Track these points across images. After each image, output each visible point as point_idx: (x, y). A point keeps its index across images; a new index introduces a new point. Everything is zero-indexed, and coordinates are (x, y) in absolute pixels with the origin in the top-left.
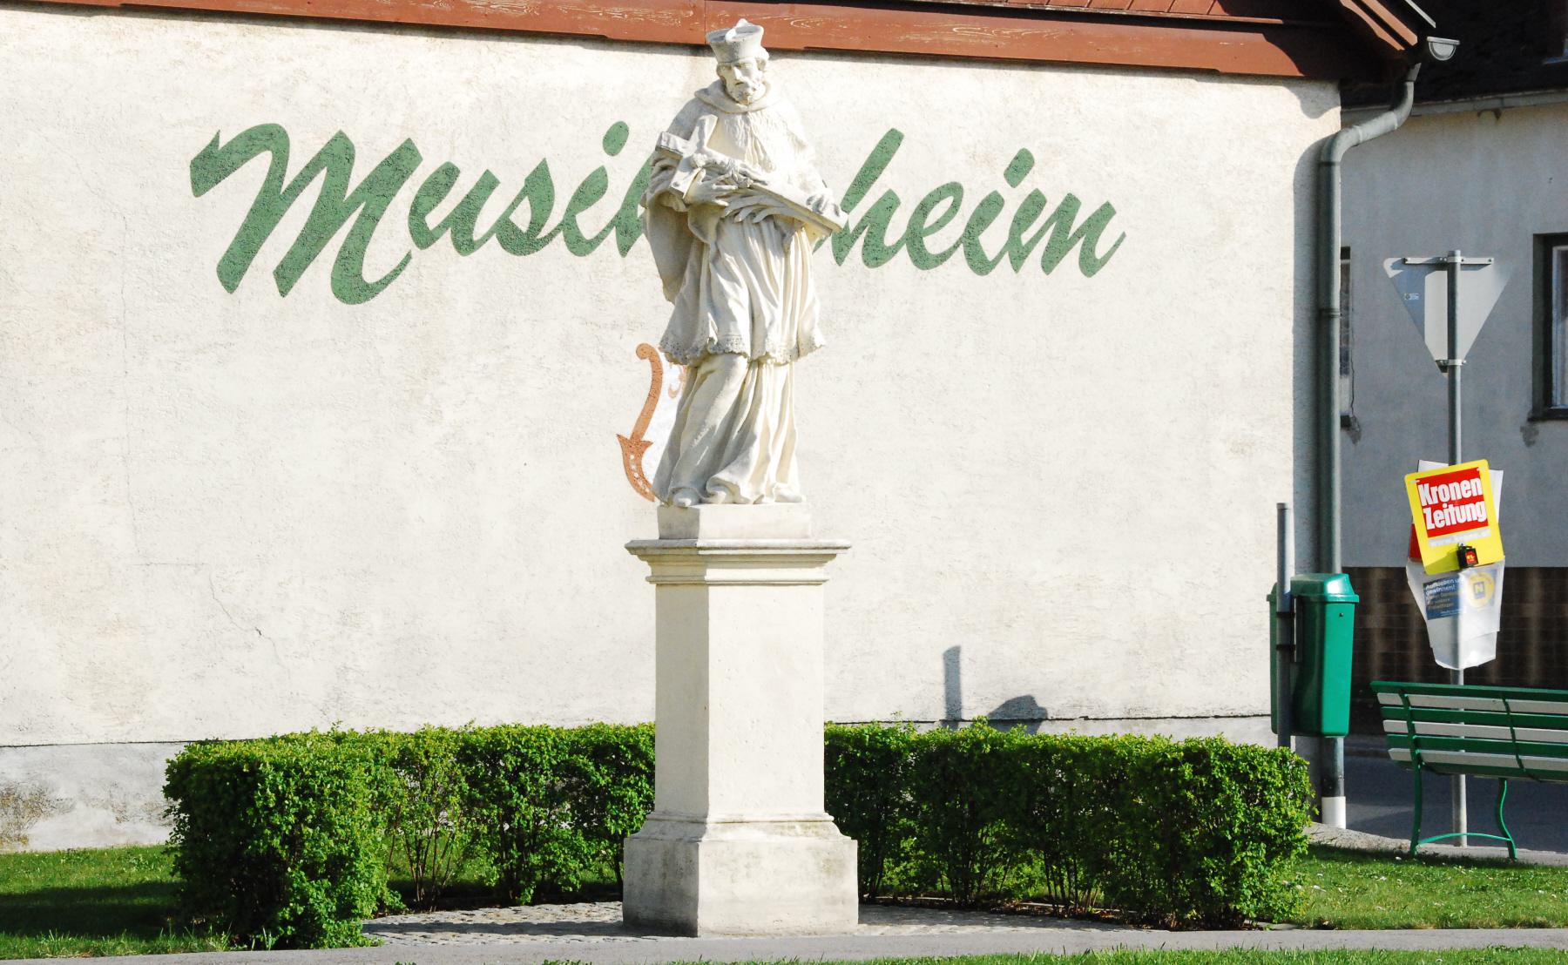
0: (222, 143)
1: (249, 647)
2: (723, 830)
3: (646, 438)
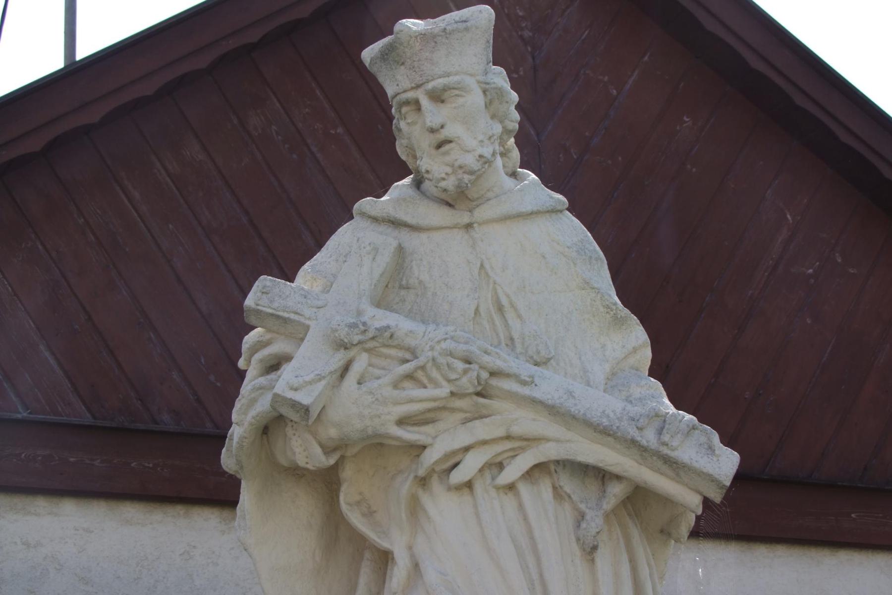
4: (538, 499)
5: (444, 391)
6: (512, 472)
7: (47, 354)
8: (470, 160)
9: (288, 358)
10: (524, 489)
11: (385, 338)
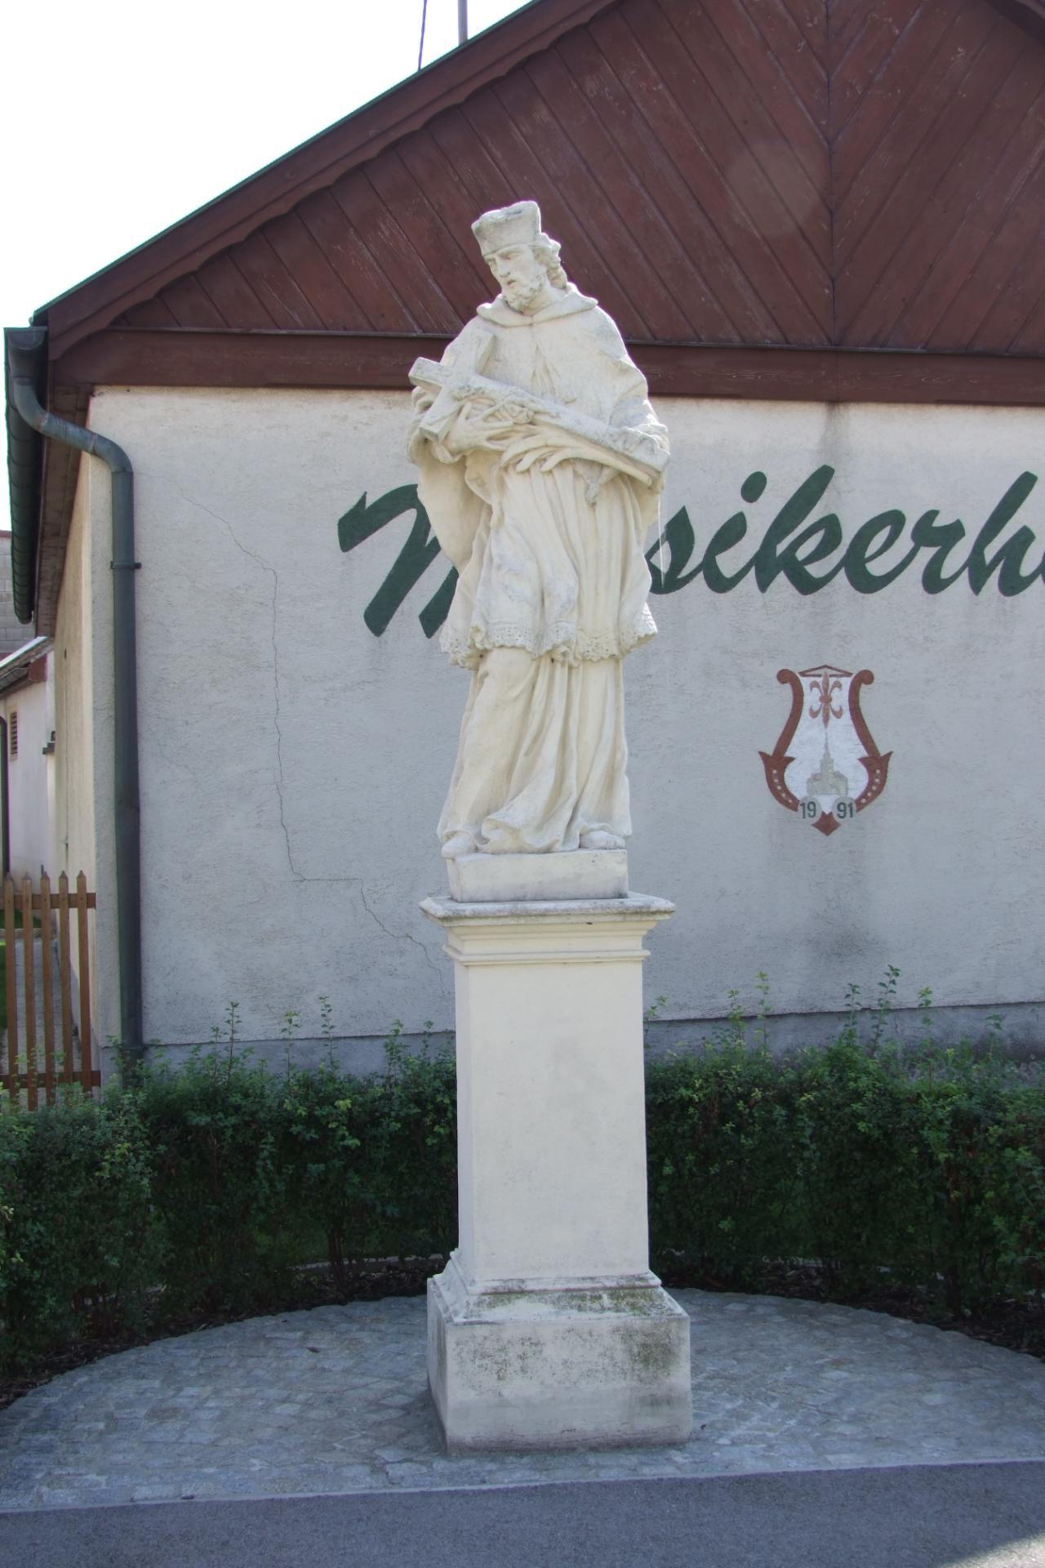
0: (369, 502)
1: (402, 953)
2: (491, 1305)
3: (788, 754)
4: (565, 477)
5: (510, 423)
6: (548, 465)
7: (434, 285)
8: (525, 292)
10: (556, 472)
11: (479, 394)
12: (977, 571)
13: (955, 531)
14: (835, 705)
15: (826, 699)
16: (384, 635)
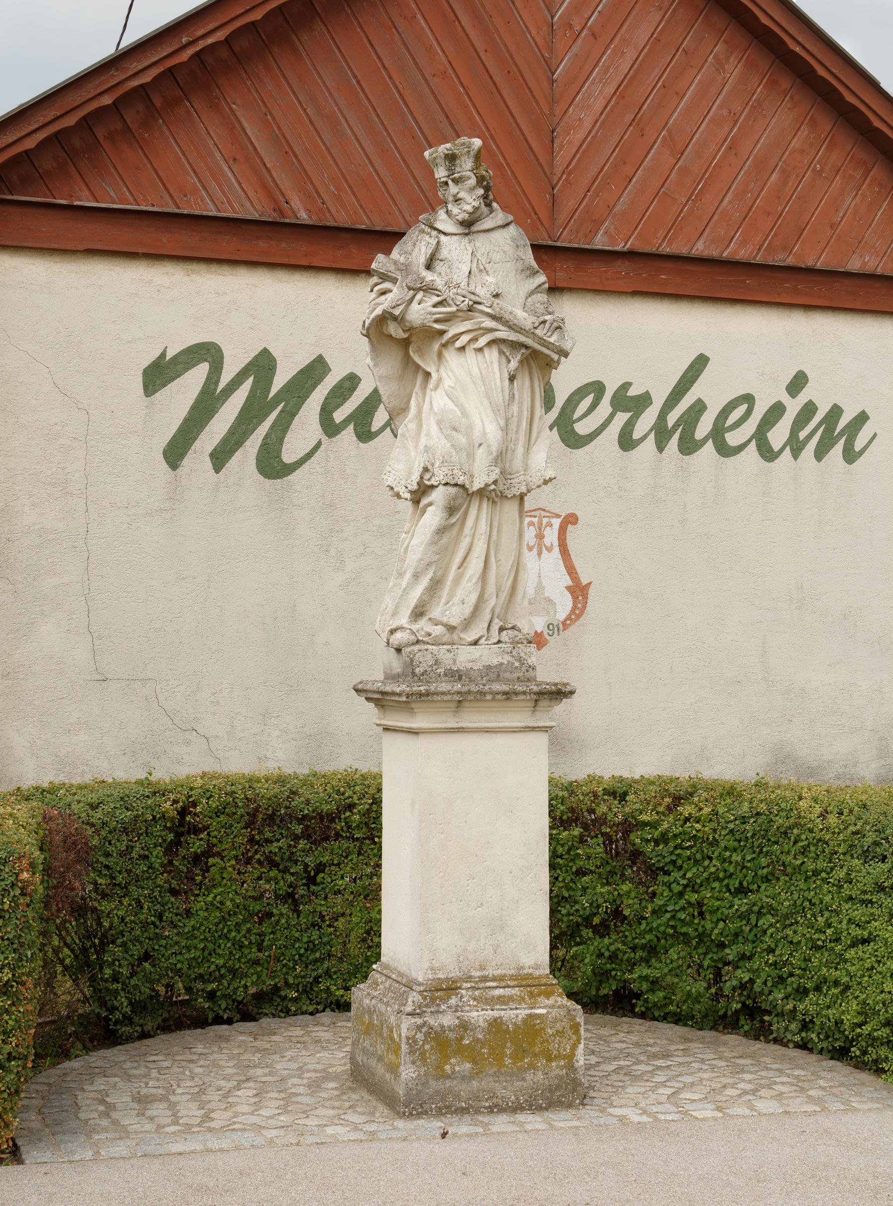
0: (170, 355)
4: (492, 355)
6: (482, 342)
9: (391, 291)
12: (662, 434)
13: (644, 400)
14: (547, 541)
15: (540, 536)
16: (178, 470)
